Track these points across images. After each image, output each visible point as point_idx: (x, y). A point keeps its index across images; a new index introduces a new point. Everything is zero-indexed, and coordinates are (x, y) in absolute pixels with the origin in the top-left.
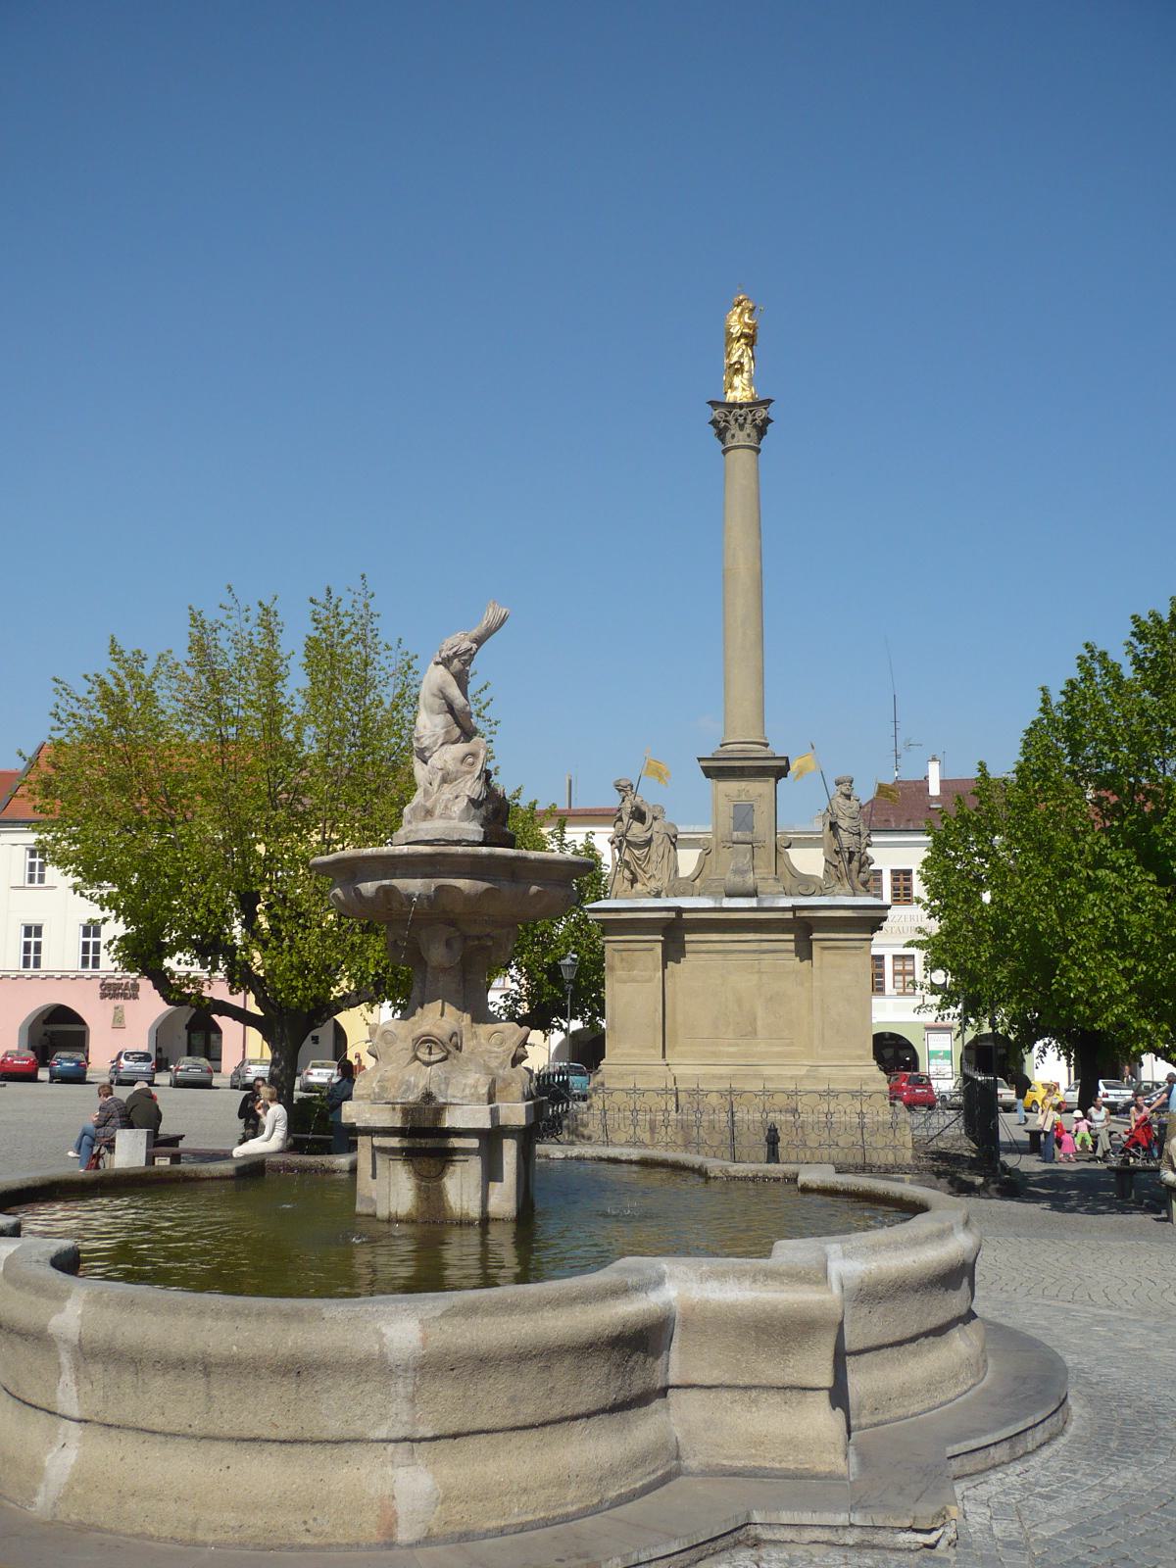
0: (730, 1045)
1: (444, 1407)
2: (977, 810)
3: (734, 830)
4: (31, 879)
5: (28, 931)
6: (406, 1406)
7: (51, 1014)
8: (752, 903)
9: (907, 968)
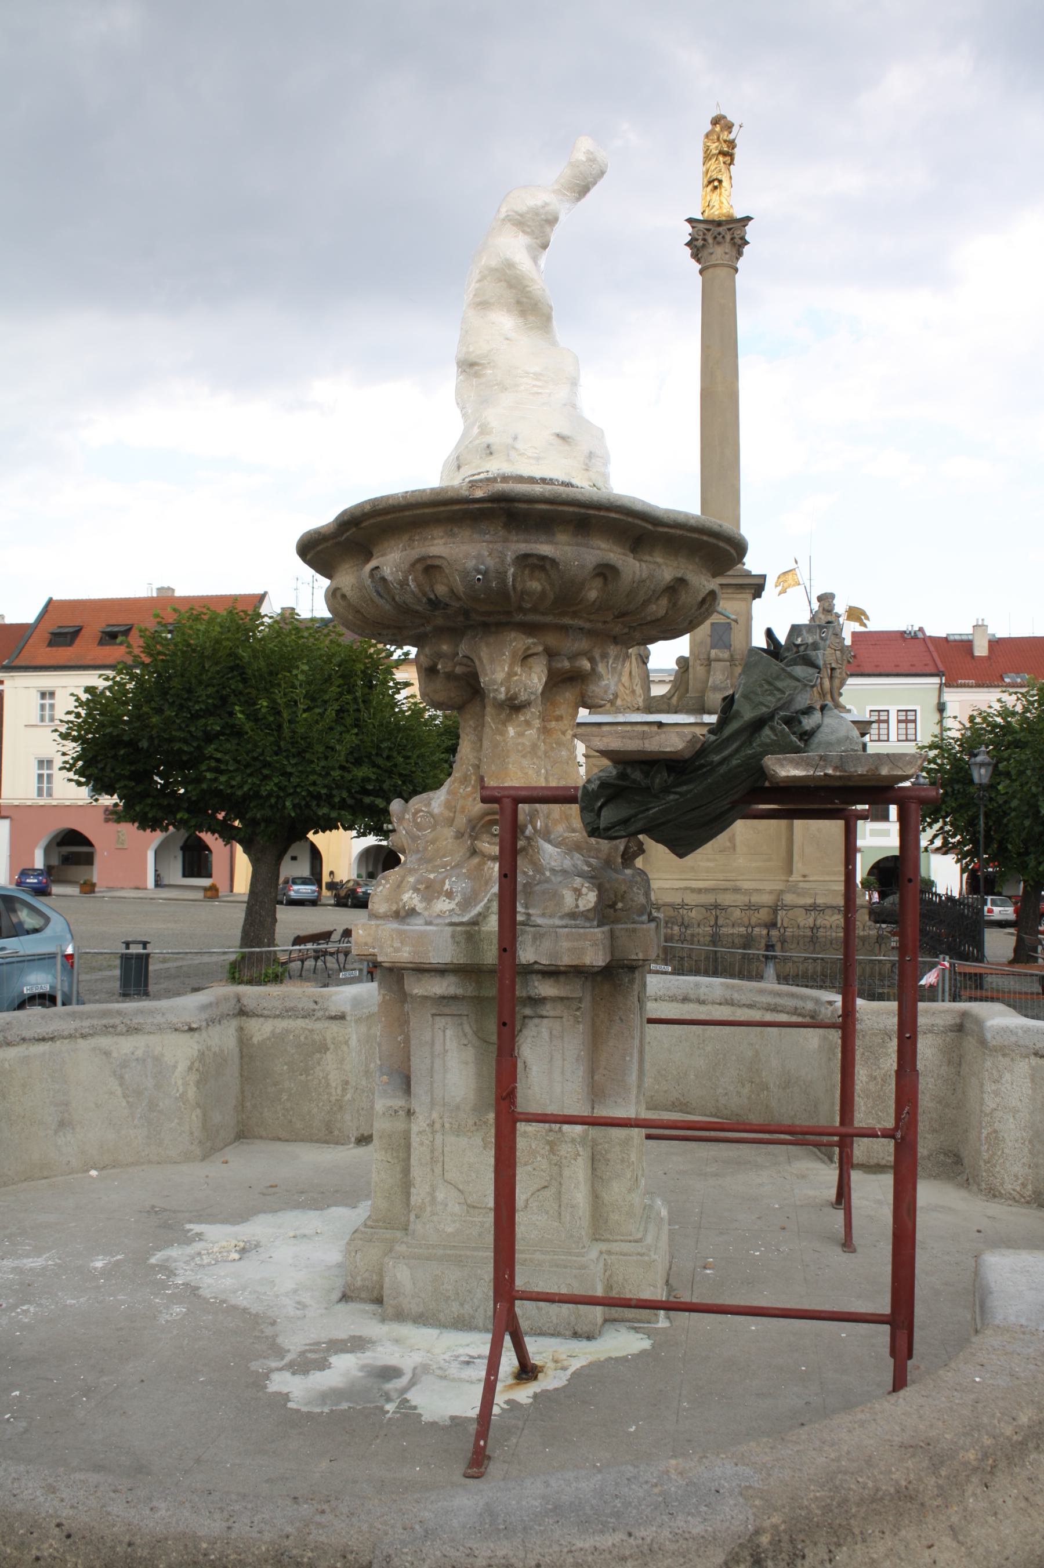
0: (708, 860)
2: (684, 1532)
3: (712, 648)
4: (42, 719)
5: (41, 763)
7: (63, 838)
9: (909, 718)
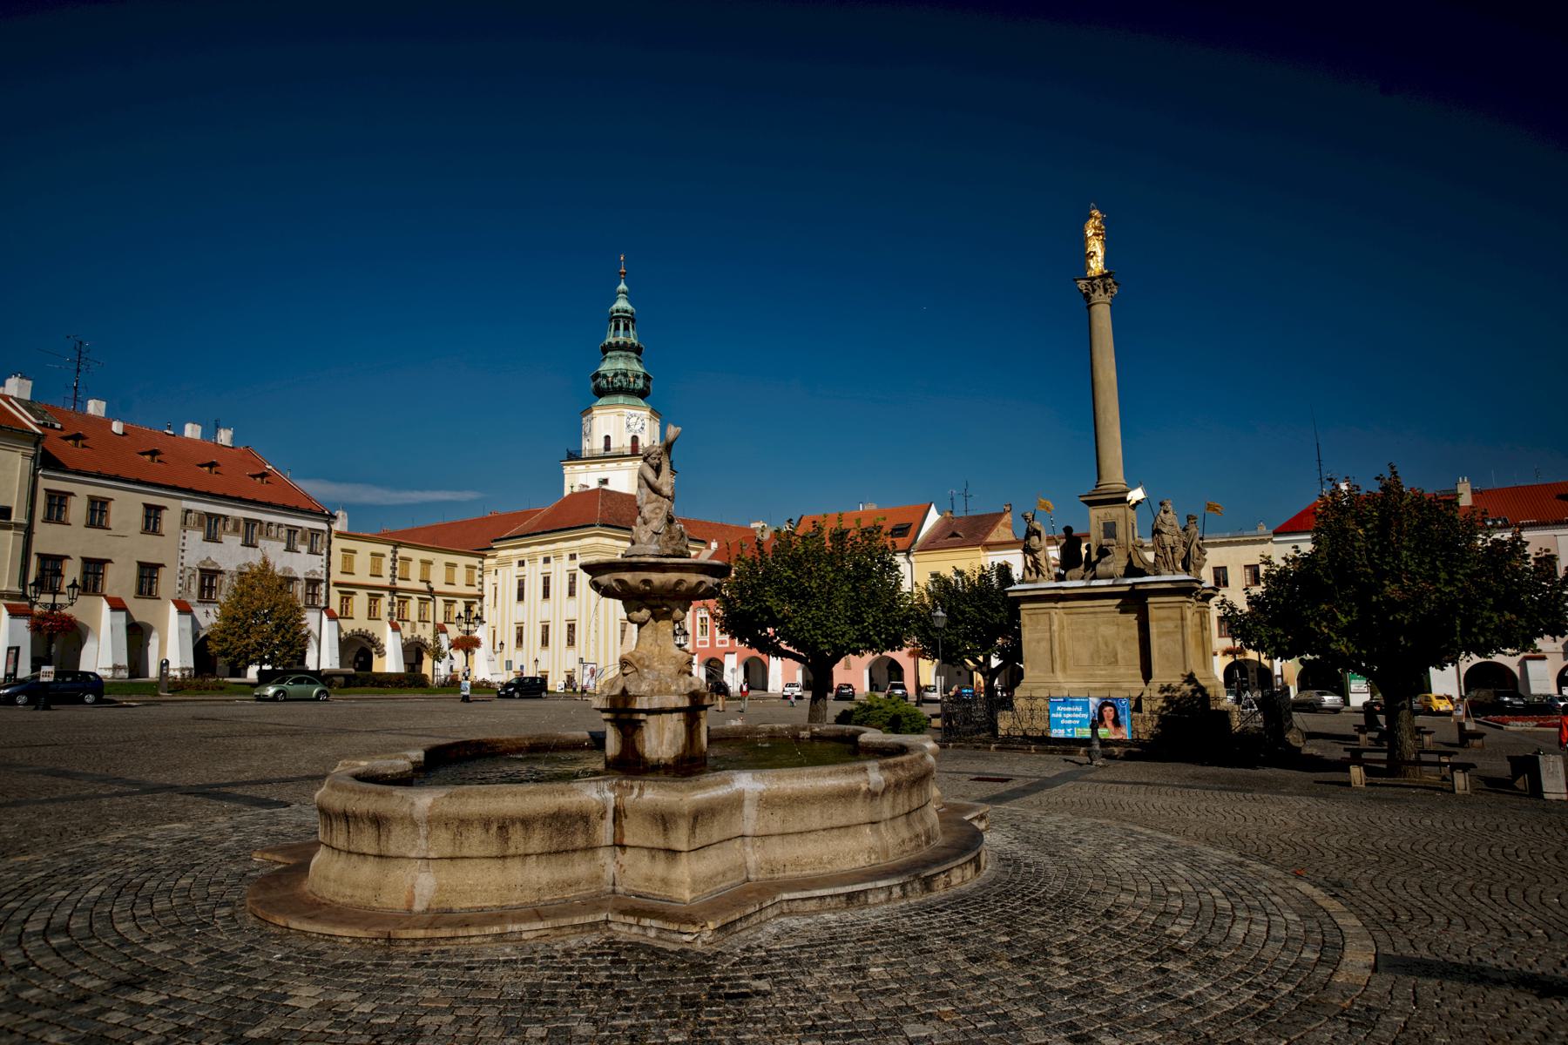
1: (443, 842)
6: (424, 841)
8: (1110, 582)
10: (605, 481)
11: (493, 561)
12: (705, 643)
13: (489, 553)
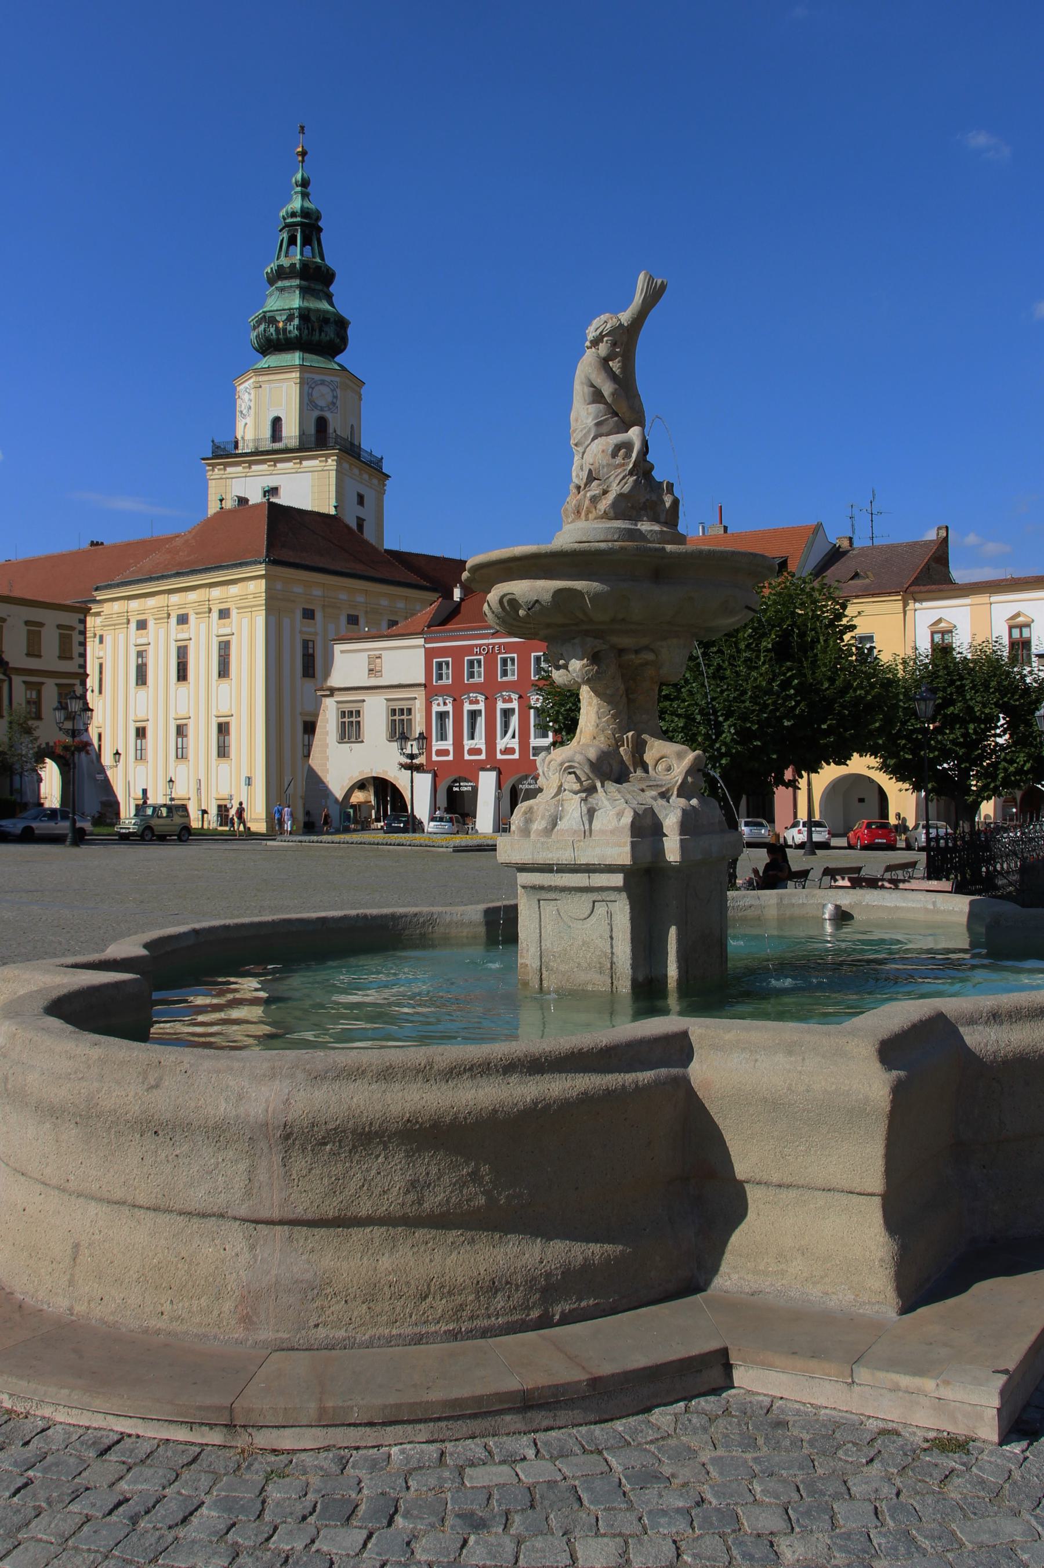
10: (274, 491)
11: (99, 620)
12: (445, 753)
13: (95, 608)
